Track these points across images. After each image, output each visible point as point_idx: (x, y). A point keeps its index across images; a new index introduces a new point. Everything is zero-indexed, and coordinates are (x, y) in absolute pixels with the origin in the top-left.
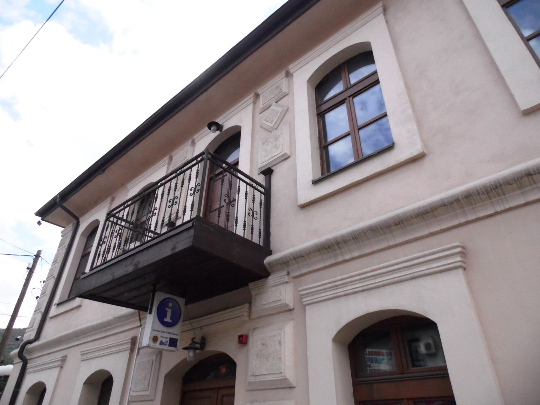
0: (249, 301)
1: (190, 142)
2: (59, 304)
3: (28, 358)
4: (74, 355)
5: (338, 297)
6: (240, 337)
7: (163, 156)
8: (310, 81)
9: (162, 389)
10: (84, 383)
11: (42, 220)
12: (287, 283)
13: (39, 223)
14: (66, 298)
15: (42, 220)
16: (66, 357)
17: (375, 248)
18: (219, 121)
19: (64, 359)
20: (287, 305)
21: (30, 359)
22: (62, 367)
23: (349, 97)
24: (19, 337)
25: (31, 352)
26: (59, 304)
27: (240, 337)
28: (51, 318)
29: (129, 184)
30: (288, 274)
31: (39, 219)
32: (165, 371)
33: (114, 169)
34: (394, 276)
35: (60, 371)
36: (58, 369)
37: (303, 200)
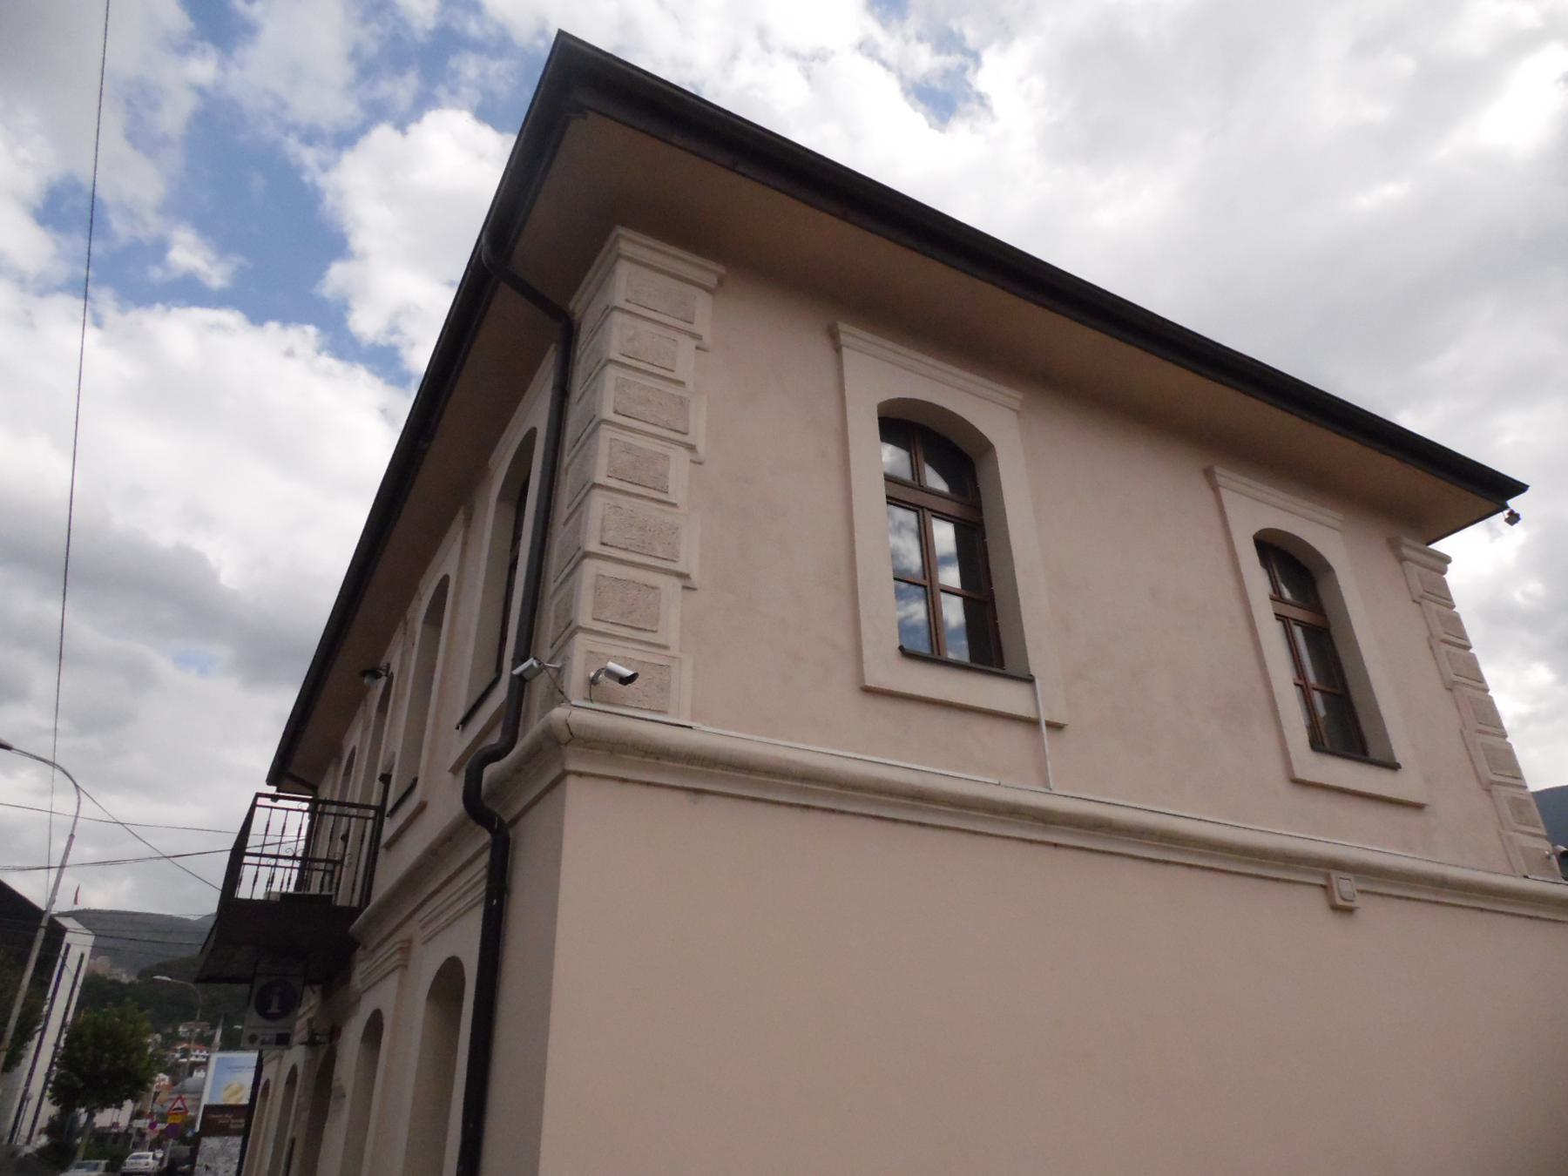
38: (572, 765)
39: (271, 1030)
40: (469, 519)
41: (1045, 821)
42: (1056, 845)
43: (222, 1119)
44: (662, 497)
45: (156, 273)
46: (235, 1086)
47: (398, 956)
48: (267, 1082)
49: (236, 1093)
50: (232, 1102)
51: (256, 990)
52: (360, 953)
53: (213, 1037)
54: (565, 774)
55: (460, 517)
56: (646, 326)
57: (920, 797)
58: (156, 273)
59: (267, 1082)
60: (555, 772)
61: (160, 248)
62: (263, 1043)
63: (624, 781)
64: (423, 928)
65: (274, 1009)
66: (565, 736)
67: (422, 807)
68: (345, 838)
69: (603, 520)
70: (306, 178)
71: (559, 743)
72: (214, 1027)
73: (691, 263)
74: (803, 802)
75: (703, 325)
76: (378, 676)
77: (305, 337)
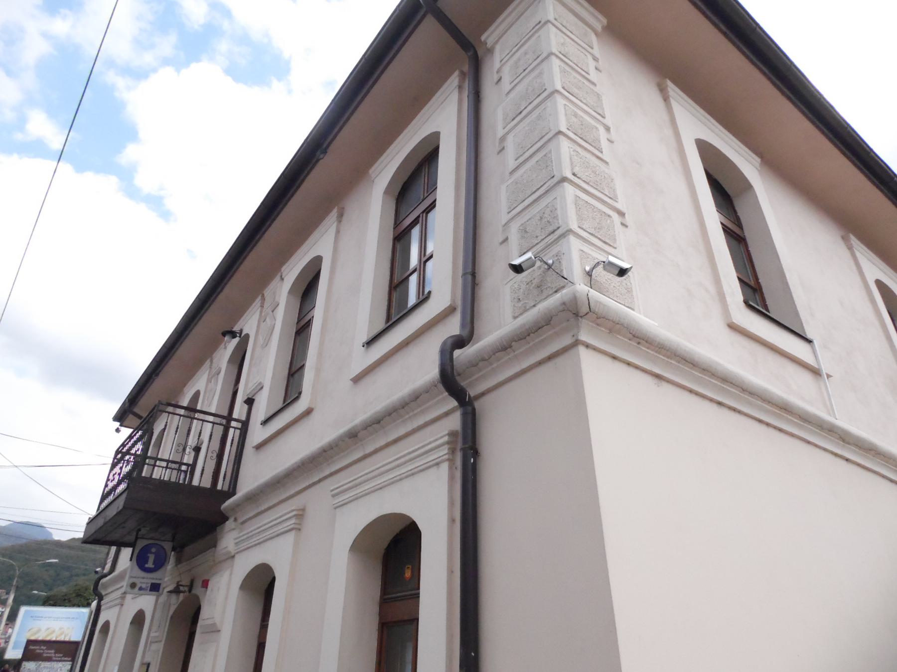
0: (214, 545)
1: (278, 278)
2: (265, 422)
3: (103, 593)
4: (317, 499)
5: (259, 544)
6: (203, 581)
7: (327, 212)
8: (387, 191)
9: (233, 613)
10: (131, 623)
11: (121, 425)
12: (234, 529)
13: (118, 430)
14: (380, 325)
15: (121, 425)
16: (303, 510)
17: (525, 364)
18: (236, 329)
19: (300, 515)
20: (230, 552)
21: (483, 394)
22: (122, 605)
23: (423, 212)
24: (98, 569)
25: (106, 586)
26: (265, 422)
27: (203, 581)
28: (259, 447)
29: (284, 267)
30: (235, 520)
31: (117, 424)
32: (171, 612)
33: (230, 290)
34: (374, 484)
35: (120, 609)
36: (117, 608)
37: (357, 368)
38: (584, 337)
39: (146, 579)
40: (341, 216)
41: (844, 441)
42: (847, 460)
43: (38, 649)
44: (599, 155)
45: (19, 136)
46: (35, 630)
47: (293, 521)
48: (107, 625)
49: (35, 634)
50: (48, 638)
51: (137, 551)
52: (230, 524)
53: (7, 599)
54: (576, 343)
55: (334, 213)
56: (569, 40)
57: (785, 409)
58: (19, 136)
59: (107, 625)
60: (567, 340)
61: (21, 123)
62: (141, 589)
63: (614, 358)
64: (333, 496)
65: (150, 565)
66: (584, 309)
67: (308, 412)
68: (197, 450)
69: (571, 159)
70: (117, 94)
71: (577, 315)
72: (8, 593)
73: (586, 9)
74: (720, 399)
75: (596, 51)
76: (234, 337)
77: (112, 181)
